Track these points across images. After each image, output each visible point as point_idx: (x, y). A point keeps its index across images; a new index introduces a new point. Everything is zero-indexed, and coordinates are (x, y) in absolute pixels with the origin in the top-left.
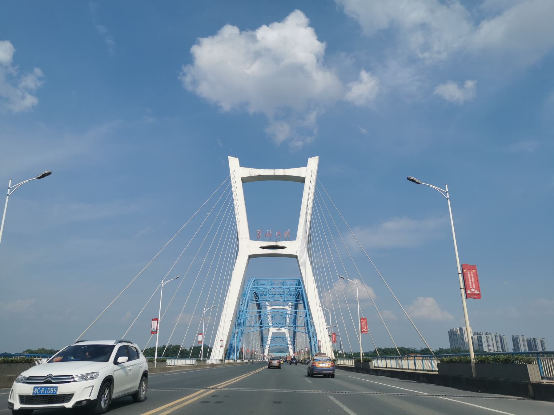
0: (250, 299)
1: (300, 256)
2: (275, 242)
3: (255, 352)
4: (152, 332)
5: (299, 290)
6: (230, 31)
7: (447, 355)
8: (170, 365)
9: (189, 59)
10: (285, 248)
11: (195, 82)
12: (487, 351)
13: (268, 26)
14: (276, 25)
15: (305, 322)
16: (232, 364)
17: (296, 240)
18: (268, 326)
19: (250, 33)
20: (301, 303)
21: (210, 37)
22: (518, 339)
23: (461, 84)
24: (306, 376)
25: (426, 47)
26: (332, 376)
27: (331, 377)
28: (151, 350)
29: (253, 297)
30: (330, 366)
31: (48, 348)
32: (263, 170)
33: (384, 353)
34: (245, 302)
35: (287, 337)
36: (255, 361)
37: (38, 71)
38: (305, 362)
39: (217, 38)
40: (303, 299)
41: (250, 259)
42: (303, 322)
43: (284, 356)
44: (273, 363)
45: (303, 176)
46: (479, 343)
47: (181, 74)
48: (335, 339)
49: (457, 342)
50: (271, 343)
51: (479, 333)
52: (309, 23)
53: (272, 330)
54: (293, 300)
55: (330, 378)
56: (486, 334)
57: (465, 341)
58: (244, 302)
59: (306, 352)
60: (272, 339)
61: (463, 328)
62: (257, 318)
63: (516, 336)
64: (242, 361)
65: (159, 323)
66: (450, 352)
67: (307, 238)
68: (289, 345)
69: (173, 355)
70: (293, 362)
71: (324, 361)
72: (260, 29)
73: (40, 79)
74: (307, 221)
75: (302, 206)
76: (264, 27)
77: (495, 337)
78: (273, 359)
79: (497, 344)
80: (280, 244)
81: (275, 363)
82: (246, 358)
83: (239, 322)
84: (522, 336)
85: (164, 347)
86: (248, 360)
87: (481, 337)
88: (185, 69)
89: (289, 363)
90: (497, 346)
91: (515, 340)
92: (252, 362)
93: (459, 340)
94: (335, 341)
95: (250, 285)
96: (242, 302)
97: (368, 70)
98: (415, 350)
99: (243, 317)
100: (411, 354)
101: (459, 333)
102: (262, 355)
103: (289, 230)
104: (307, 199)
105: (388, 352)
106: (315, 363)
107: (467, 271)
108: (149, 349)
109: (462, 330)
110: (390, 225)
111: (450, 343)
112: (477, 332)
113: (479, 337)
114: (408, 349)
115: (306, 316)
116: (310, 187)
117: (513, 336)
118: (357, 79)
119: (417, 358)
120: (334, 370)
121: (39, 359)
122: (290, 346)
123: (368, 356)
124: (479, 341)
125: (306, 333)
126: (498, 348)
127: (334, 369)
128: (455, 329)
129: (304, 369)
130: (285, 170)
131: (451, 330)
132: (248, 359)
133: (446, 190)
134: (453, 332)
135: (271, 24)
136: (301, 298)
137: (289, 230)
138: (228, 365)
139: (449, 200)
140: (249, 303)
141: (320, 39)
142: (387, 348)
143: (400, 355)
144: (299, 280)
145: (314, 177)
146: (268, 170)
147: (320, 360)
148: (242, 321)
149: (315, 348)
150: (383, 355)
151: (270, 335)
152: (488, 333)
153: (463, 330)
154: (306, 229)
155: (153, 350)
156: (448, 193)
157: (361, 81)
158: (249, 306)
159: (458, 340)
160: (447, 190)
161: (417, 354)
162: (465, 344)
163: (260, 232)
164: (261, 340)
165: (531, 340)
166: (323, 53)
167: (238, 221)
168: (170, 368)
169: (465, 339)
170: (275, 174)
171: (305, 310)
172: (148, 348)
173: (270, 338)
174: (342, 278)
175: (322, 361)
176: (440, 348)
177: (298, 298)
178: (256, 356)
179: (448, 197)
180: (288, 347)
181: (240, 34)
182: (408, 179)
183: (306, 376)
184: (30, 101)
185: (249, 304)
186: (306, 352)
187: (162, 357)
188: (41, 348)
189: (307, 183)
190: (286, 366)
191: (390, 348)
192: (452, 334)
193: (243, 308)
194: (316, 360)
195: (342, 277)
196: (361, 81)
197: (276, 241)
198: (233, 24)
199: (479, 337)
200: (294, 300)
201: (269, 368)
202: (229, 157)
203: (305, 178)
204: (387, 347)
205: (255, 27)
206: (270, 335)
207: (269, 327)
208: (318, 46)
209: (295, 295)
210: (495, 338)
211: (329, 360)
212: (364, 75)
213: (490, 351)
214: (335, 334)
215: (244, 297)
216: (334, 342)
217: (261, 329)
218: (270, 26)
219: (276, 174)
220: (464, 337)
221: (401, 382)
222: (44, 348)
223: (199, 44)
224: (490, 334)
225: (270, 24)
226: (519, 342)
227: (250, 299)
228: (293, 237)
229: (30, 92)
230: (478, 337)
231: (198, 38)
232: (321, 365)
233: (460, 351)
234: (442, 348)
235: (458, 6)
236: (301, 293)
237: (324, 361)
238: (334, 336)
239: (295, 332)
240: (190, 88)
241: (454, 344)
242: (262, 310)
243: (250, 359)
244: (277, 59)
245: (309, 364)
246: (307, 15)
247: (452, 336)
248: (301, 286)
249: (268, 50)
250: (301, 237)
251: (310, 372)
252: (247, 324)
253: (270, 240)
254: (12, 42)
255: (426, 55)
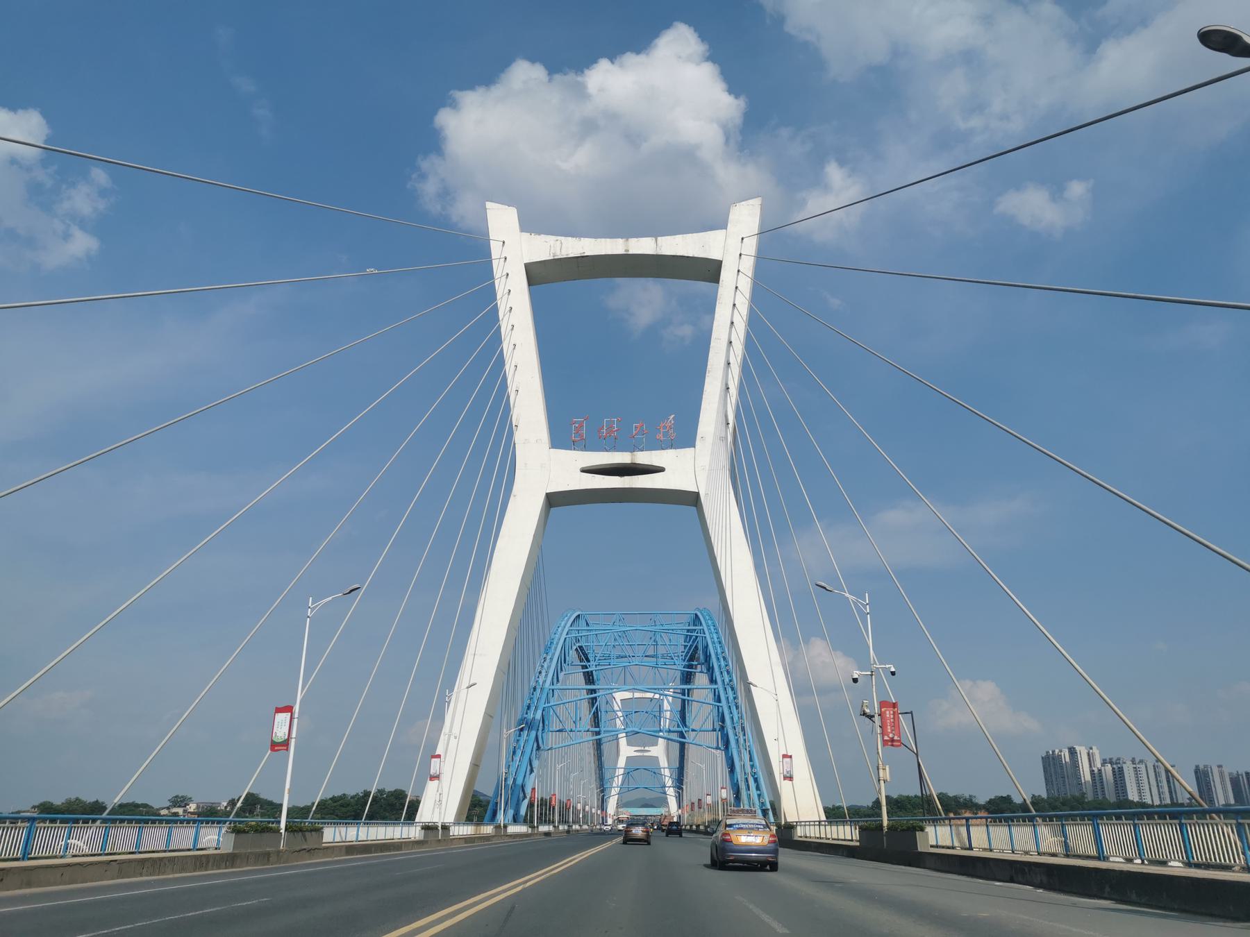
0: (565, 662)
1: (707, 494)
2: (629, 453)
3: (587, 807)
4: (274, 746)
5: (697, 637)
6: (524, 73)
7: (1141, 813)
8: (344, 840)
9: (433, 142)
10: (660, 470)
11: (446, 194)
12: (1136, 799)
13: (612, 62)
14: (630, 58)
15: (716, 719)
16: (487, 838)
17: (726, 229)
18: (614, 729)
19: (571, 77)
20: (701, 672)
21: (481, 91)
22: (1210, 774)
23: (1057, 191)
24: (706, 866)
25: (976, 106)
26: (774, 867)
27: (768, 867)
28: (335, 802)
29: (573, 655)
30: (766, 841)
31: (89, 798)
32: (592, 240)
33: (898, 807)
34: (549, 667)
35: (664, 768)
36: (575, 827)
37: (100, 175)
38: (706, 831)
39: (497, 91)
40: (706, 661)
41: (552, 509)
42: (711, 718)
43: (654, 816)
44: (633, 832)
45: (715, 255)
46: (1116, 781)
47: (414, 176)
48: (896, 725)
49: (1064, 782)
50: (622, 784)
51: (1114, 760)
52: (708, 54)
53: (626, 751)
54: (680, 665)
55: (767, 871)
56: (1133, 761)
57: (1082, 778)
58: (546, 666)
59: (722, 800)
60: (627, 774)
61: (1078, 748)
62: (585, 704)
63: (1206, 766)
64: (530, 829)
65: (295, 721)
66: (1058, 804)
67: (730, 438)
68: (667, 789)
69: (387, 814)
70: (674, 830)
71: (752, 829)
72: (593, 68)
73: (103, 193)
74: (728, 388)
75: (712, 344)
76: (604, 64)
77: (1155, 769)
78: (633, 822)
79: (1158, 786)
80: (643, 458)
81: (638, 831)
82: (544, 820)
83: (531, 716)
84: (1220, 766)
85: (367, 794)
86: (554, 826)
87: (1121, 769)
88: (425, 165)
89: (664, 834)
90: (1159, 791)
91: (1202, 776)
92: (568, 832)
93: (1068, 777)
94: (896, 738)
95: (566, 624)
96: (542, 666)
97: (842, 163)
98: (974, 800)
99: (542, 705)
100: (963, 811)
101: (1068, 760)
102: (599, 812)
103: (673, 416)
104: (729, 322)
105: (909, 806)
106: (729, 835)
107: (886, 711)
108: (330, 799)
109: (1076, 753)
110: (894, 517)
111: (1046, 784)
112: (1111, 757)
113: (1116, 770)
114: (956, 798)
115: (719, 700)
116: (732, 323)
117: (1197, 767)
118: (818, 182)
119: (975, 820)
120: (776, 852)
121: (107, 827)
122: (671, 792)
123: (858, 814)
124: (1118, 776)
125: (720, 749)
126: (1162, 796)
127: (777, 850)
128: (1057, 751)
129: (702, 850)
130: (659, 238)
131: (1048, 752)
132: (553, 822)
133: (865, 601)
134: (1053, 759)
135: (618, 58)
136: (702, 658)
137: (673, 416)
138: (466, 842)
139: (869, 616)
140: (561, 670)
141: (734, 88)
142: (904, 796)
143: (1033, 811)
144: (696, 614)
145: (748, 265)
146: (608, 240)
147: (742, 826)
148: (538, 716)
149: (749, 790)
150: (896, 812)
151: (622, 762)
152: (1137, 761)
153: (1078, 753)
154: (726, 411)
155: (338, 801)
156: (868, 606)
157: (826, 188)
158: (560, 678)
159: (1066, 778)
160: (867, 602)
161: (976, 809)
162: (1084, 787)
163: (581, 425)
164: (598, 775)
165: (1240, 777)
166: (738, 121)
167: (514, 389)
168: (332, 849)
169: (1082, 775)
170: (628, 251)
171: (715, 686)
172: (328, 798)
173: (621, 771)
174: (825, 588)
175: (746, 829)
176: (1033, 795)
177: (691, 659)
178: (581, 816)
179: (868, 611)
180: (665, 793)
181: (550, 81)
182: (817, 585)
183: (706, 866)
184: (82, 243)
185: (561, 676)
186: (722, 800)
187: (309, 820)
188: (73, 797)
189: (727, 275)
190: (659, 841)
191: (913, 795)
192: (1051, 763)
193: (545, 681)
194: (730, 826)
195: (823, 584)
196: (826, 188)
197: (633, 449)
198: (533, 60)
199: (1116, 770)
200: (684, 663)
201: (625, 842)
202: (489, 205)
203: (721, 262)
204: (905, 793)
205: (583, 62)
206: (622, 762)
207: (617, 733)
208: (727, 105)
209: (684, 654)
210: (1155, 771)
211: (764, 828)
212: (834, 173)
213: (1144, 801)
214: (894, 705)
215: (547, 653)
216: (892, 740)
217: (598, 737)
218: (617, 61)
219: (630, 252)
220: (1081, 770)
221: (1101, 911)
222: (80, 798)
223: (454, 105)
224: (1141, 761)
225: (616, 59)
226: (1212, 782)
227: (565, 662)
228: (685, 437)
229: (82, 224)
230: (1113, 768)
231: (452, 92)
232: (744, 839)
233: (1083, 802)
234: (1039, 796)
235: (1048, 9)
236: (700, 647)
237: (752, 829)
238: (889, 713)
239: (682, 746)
240: (435, 208)
241: (1055, 786)
242: (598, 687)
243: (559, 822)
244: (633, 136)
245: (714, 835)
246: (703, 36)
247: (1052, 767)
248: (701, 628)
249: (612, 117)
250: (710, 439)
251: (718, 858)
252: (556, 725)
253: (614, 448)
254: (45, 114)
255: (975, 122)
